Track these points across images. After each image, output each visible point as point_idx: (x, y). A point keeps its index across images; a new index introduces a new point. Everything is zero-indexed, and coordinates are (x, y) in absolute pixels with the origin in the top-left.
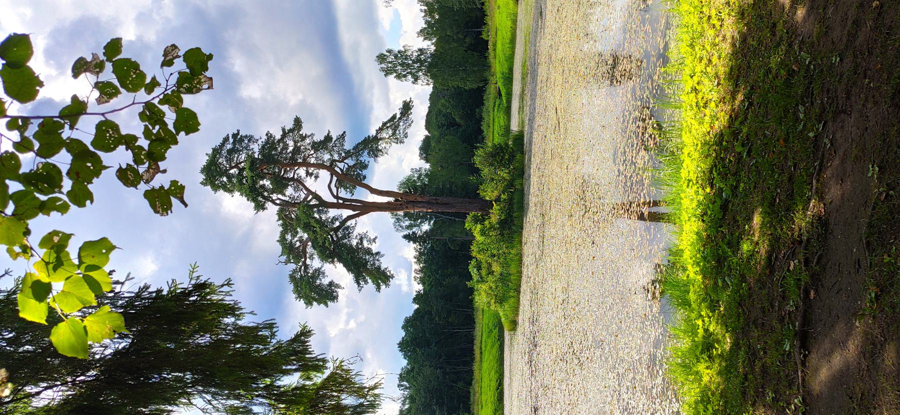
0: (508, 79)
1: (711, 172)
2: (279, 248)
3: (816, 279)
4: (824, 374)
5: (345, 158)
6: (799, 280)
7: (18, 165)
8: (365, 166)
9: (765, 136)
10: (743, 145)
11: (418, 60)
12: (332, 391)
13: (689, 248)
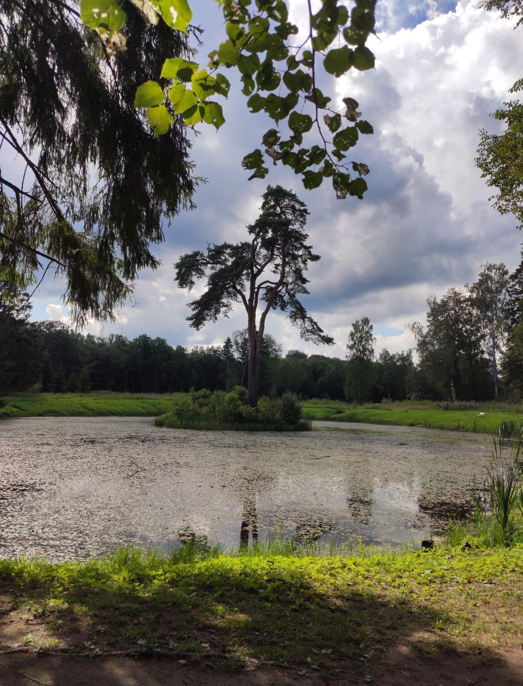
0: (351, 419)
1: (280, 580)
2: (220, 244)
3: (194, 664)
4: (119, 672)
5: (289, 293)
6: (194, 651)
7: (278, 59)
8: (283, 308)
9: (308, 623)
10: (301, 605)
11: (365, 349)
12: (109, 284)
13: (220, 563)
